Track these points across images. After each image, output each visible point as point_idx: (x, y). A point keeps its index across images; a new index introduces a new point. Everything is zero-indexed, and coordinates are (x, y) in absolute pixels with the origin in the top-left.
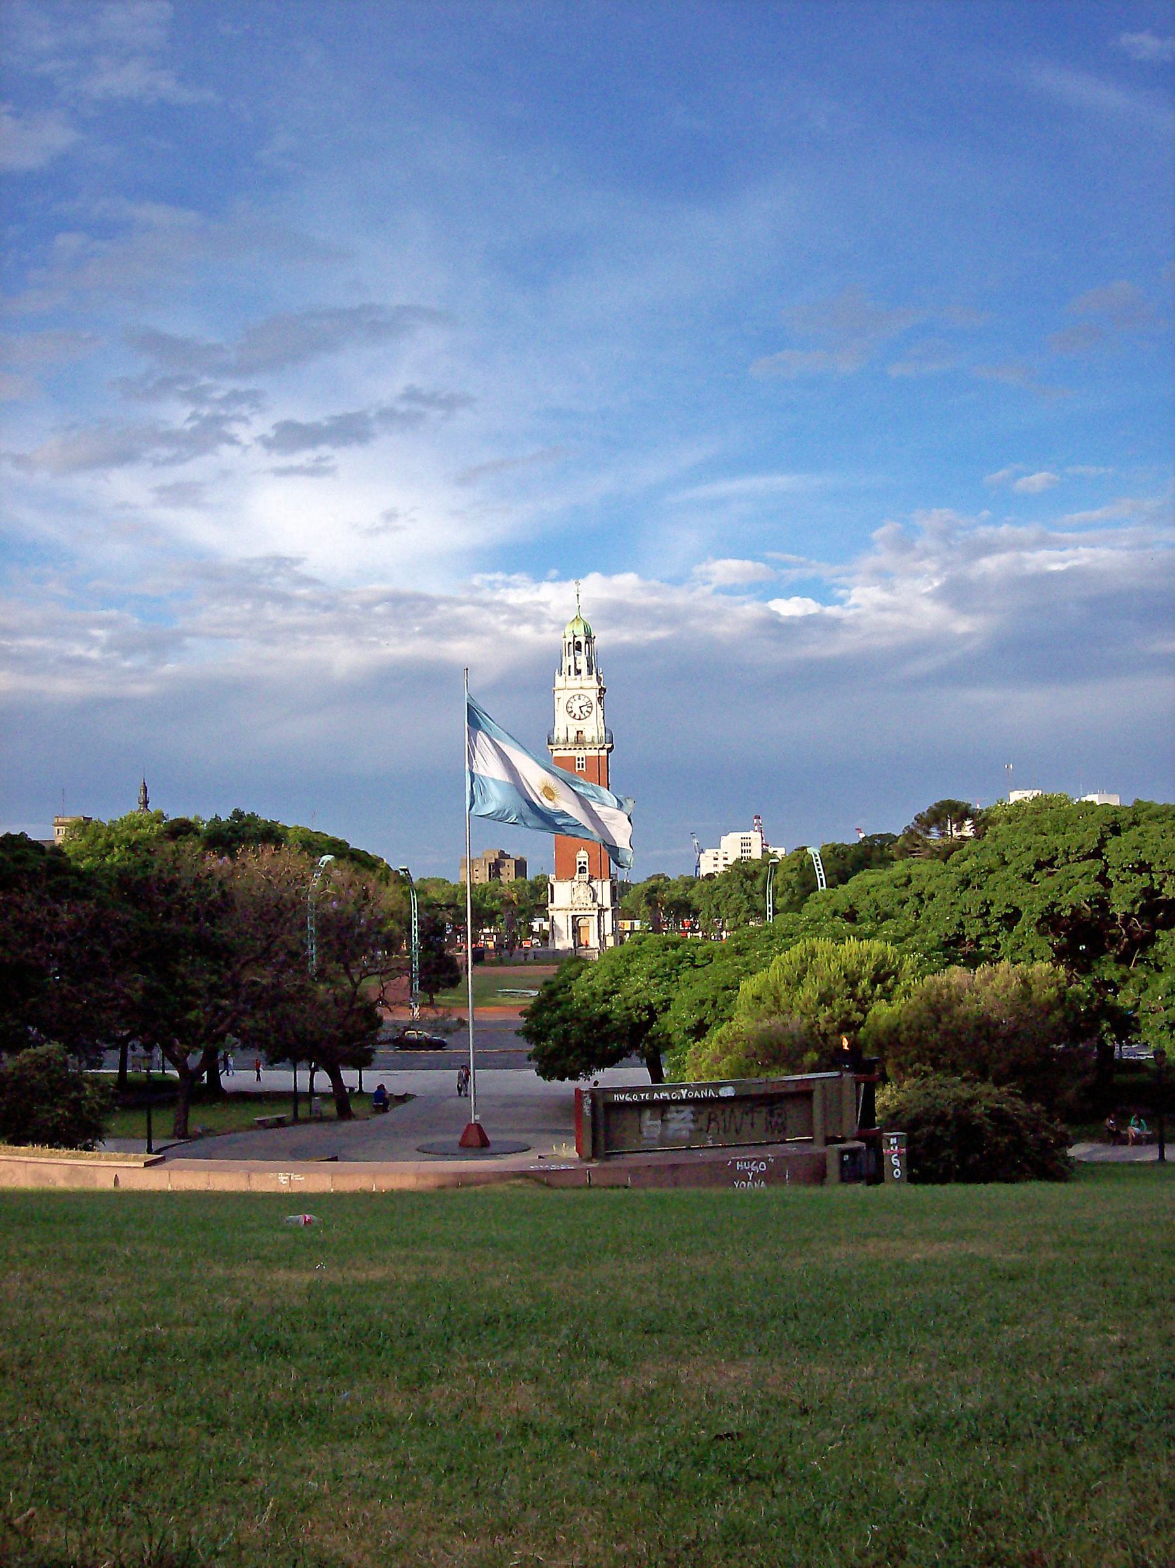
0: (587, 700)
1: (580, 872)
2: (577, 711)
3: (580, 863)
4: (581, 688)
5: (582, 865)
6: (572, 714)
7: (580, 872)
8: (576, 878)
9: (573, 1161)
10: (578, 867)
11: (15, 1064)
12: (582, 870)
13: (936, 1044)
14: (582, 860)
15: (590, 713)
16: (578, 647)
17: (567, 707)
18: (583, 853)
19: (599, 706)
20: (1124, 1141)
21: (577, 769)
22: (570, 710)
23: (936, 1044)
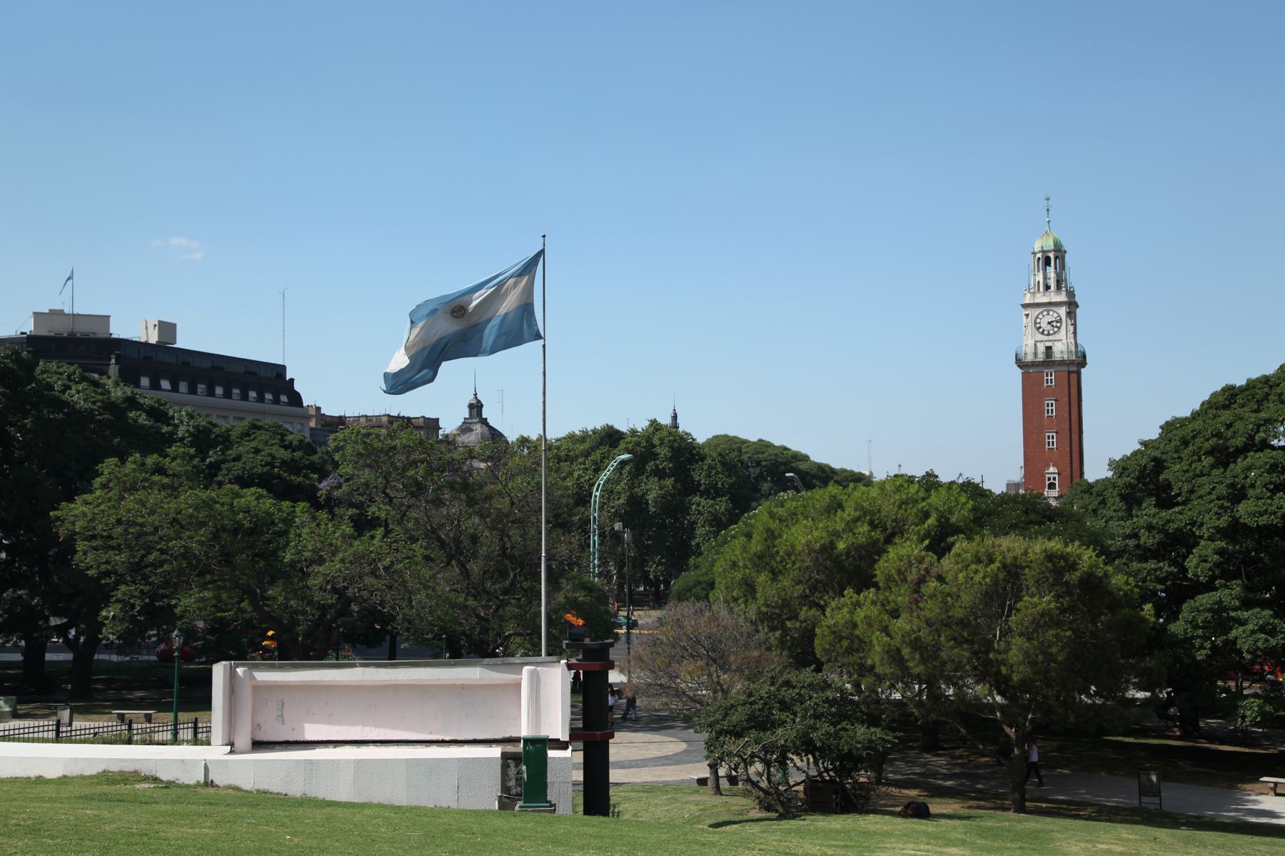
0: (1055, 315)
1: (1049, 488)
2: (1044, 325)
3: (1049, 479)
5: (1052, 481)
6: (1041, 330)
7: (1049, 488)
9: (931, 803)
10: (1048, 483)
11: (153, 460)
12: (1052, 486)
13: (284, 552)
14: (1052, 476)
15: (1059, 328)
16: (1047, 262)
17: (1035, 323)
18: (1052, 469)
19: (1069, 322)
20: (1216, 589)
21: (1047, 447)
22: (1038, 326)
23: (284, 552)
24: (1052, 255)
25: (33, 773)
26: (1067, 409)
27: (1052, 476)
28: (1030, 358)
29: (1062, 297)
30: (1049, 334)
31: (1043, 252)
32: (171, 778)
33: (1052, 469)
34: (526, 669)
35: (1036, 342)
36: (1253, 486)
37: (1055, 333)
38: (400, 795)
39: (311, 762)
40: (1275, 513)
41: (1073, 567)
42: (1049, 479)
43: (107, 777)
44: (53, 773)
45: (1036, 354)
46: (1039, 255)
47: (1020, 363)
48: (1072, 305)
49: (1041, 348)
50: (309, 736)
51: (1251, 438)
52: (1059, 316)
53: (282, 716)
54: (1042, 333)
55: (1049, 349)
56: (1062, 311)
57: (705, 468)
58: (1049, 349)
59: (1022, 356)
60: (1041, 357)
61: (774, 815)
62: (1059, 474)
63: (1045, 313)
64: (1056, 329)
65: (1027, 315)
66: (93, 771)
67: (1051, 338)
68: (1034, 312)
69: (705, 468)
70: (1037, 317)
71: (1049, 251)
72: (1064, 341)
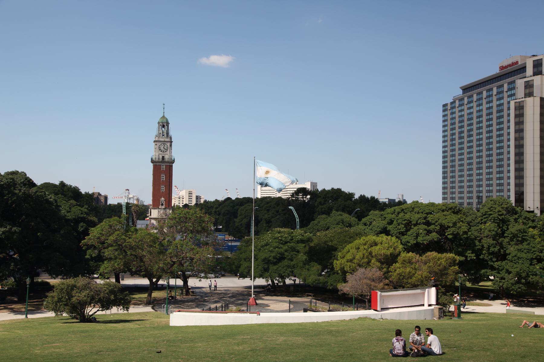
2: (162, 148)
3: (161, 202)
8: (160, 207)
10: (161, 203)
12: (162, 205)
14: (162, 201)
15: (167, 150)
16: (163, 126)
17: (159, 148)
18: (163, 199)
24: (165, 124)
25: (343, 319)
26: (169, 178)
27: (162, 201)
28: (157, 160)
29: (168, 140)
30: (163, 152)
31: (162, 123)
32: (374, 318)
33: (163, 199)
34: (427, 289)
35: (159, 154)
36: (421, 234)
37: (166, 151)
38: (406, 318)
39: (385, 313)
40: (427, 240)
41: (456, 260)
42: (161, 202)
43: (360, 319)
44: (347, 319)
45: (159, 158)
46: (161, 124)
47: (152, 161)
48: (171, 142)
49: (161, 157)
50: (389, 307)
51: (417, 222)
52: (167, 146)
53: (383, 303)
54: (161, 151)
55: (163, 157)
56: (169, 144)
57: (85, 200)
58: (163, 157)
59: (154, 159)
60: (161, 159)
61: (77, 321)
62: (165, 200)
63: (163, 144)
64: (166, 150)
65: (156, 145)
66: (356, 318)
67: (164, 153)
68: (159, 144)
69: (85, 200)
70: (160, 146)
71: (165, 123)
72: (169, 155)
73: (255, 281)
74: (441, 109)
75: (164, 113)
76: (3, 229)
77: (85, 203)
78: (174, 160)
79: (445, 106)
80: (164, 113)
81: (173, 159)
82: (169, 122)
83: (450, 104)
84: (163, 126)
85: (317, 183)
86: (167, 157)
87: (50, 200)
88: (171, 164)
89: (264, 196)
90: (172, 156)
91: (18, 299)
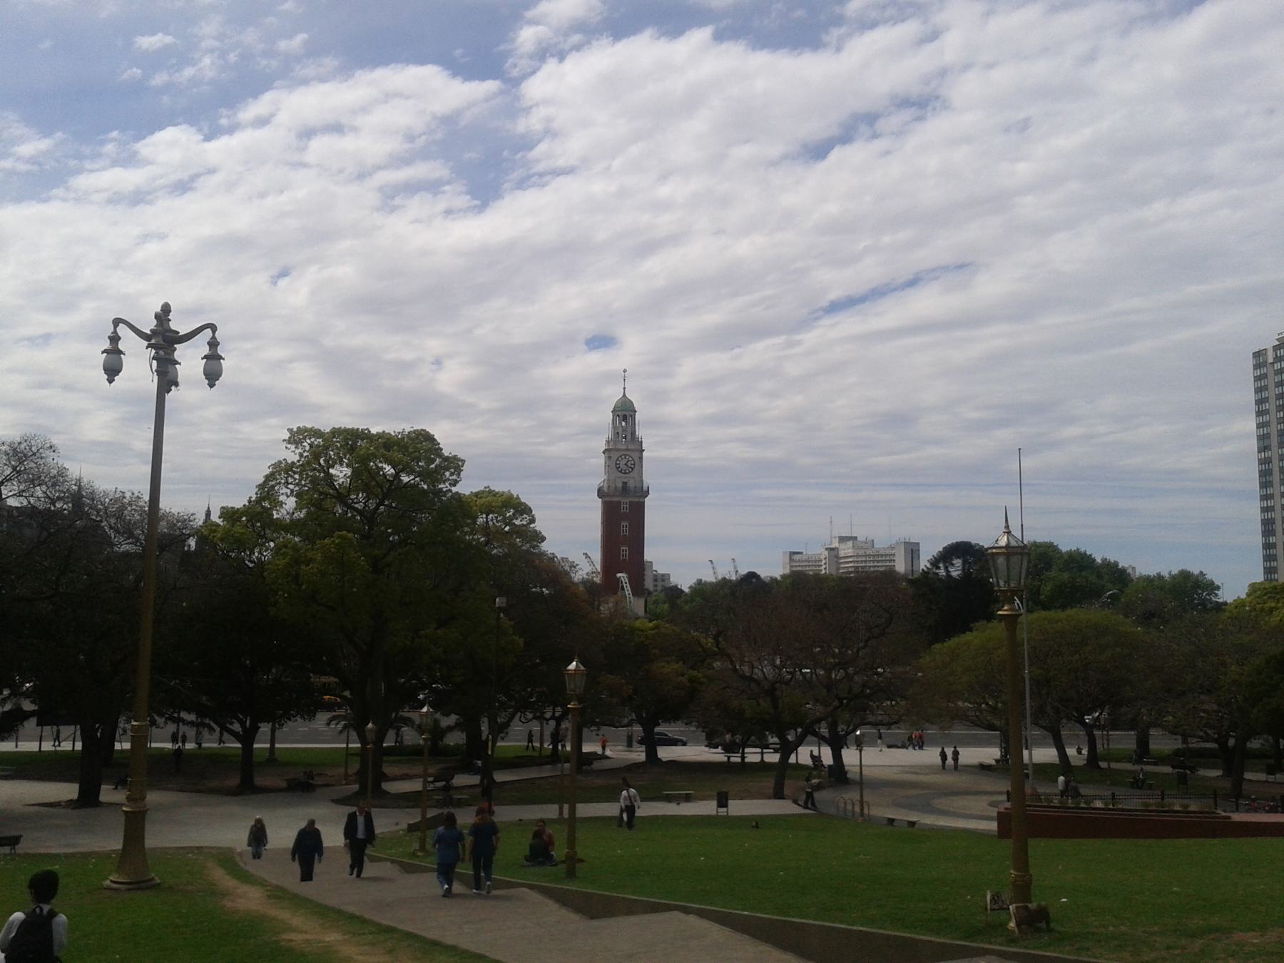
2: (622, 466)
4: (627, 450)
15: (633, 469)
17: (616, 464)
30: (625, 473)
37: (630, 472)
49: (620, 485)
54: (621, 472)
58: (625, 483)
64: (630, 470)
67: (627, 475)
70: (617, 460)
73: (206, 509)
74: (1250, 363)
75: (624, 388)
76: (349, 950)
77: (175, 528)
78: (648, 492)
79: (1257, 355)
80: (624, 388)
81: (645, 488)
82: (636, 409)
83: (1272, 349)
84: (625, 418)
85: (918, 544)
86: (631, 484)
87: (837, 678)
88: (641, 500)
89: (798, 569)
90: (642, 481)
91: (361, 744)
